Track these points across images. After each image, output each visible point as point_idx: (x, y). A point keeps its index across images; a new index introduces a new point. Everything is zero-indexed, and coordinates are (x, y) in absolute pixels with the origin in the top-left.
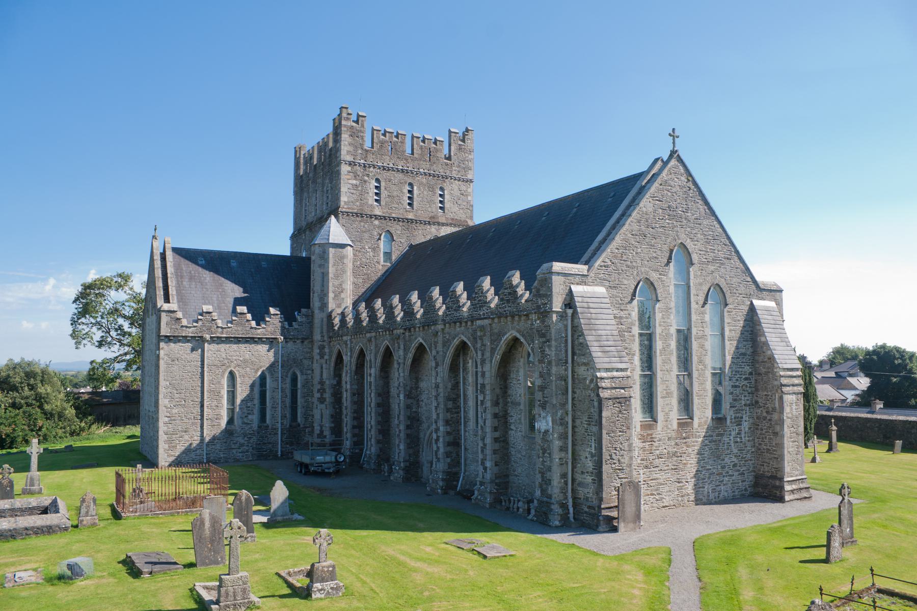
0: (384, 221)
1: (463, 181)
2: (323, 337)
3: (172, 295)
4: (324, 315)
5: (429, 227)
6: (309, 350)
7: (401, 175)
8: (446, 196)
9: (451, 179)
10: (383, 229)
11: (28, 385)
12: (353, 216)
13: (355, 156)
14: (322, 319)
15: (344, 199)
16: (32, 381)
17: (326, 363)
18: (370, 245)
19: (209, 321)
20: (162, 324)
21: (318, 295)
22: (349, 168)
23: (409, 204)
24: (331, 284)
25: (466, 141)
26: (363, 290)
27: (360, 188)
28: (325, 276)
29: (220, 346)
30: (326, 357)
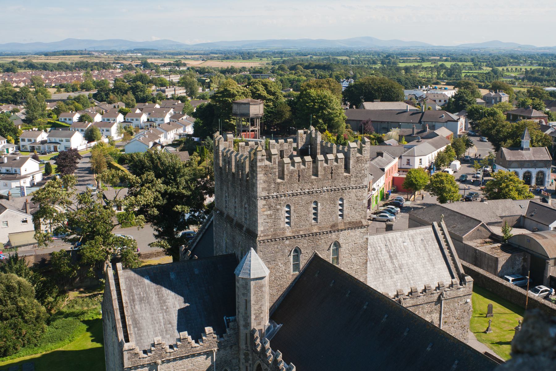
0: (293, 240)
1: (360, 188)
2: (248, 347)
3: (130, 334)
4: (248, 332)
5: (330, 235)
6: (236, 352)
7: (307, 197)
8: (345, 205)
9: (350, 189)
10: (293, 246)
11: (10, 298)
12: (268, 242)
13: (269, 191)
14: (246, 334)
15: (260, 228)
16: (12, 295)
17: (250, 366)
18: (282, 262)
19: (159, 350)
20: (125, 360)
21: (243, 316)
22: (264, 202)
23: (315, 219)
24: (252, 309)
25: (363, 152)
26: (277, 297)
27: (273, 217)
28: (247, 303)
29: (169, 364)
30: (250, 362)
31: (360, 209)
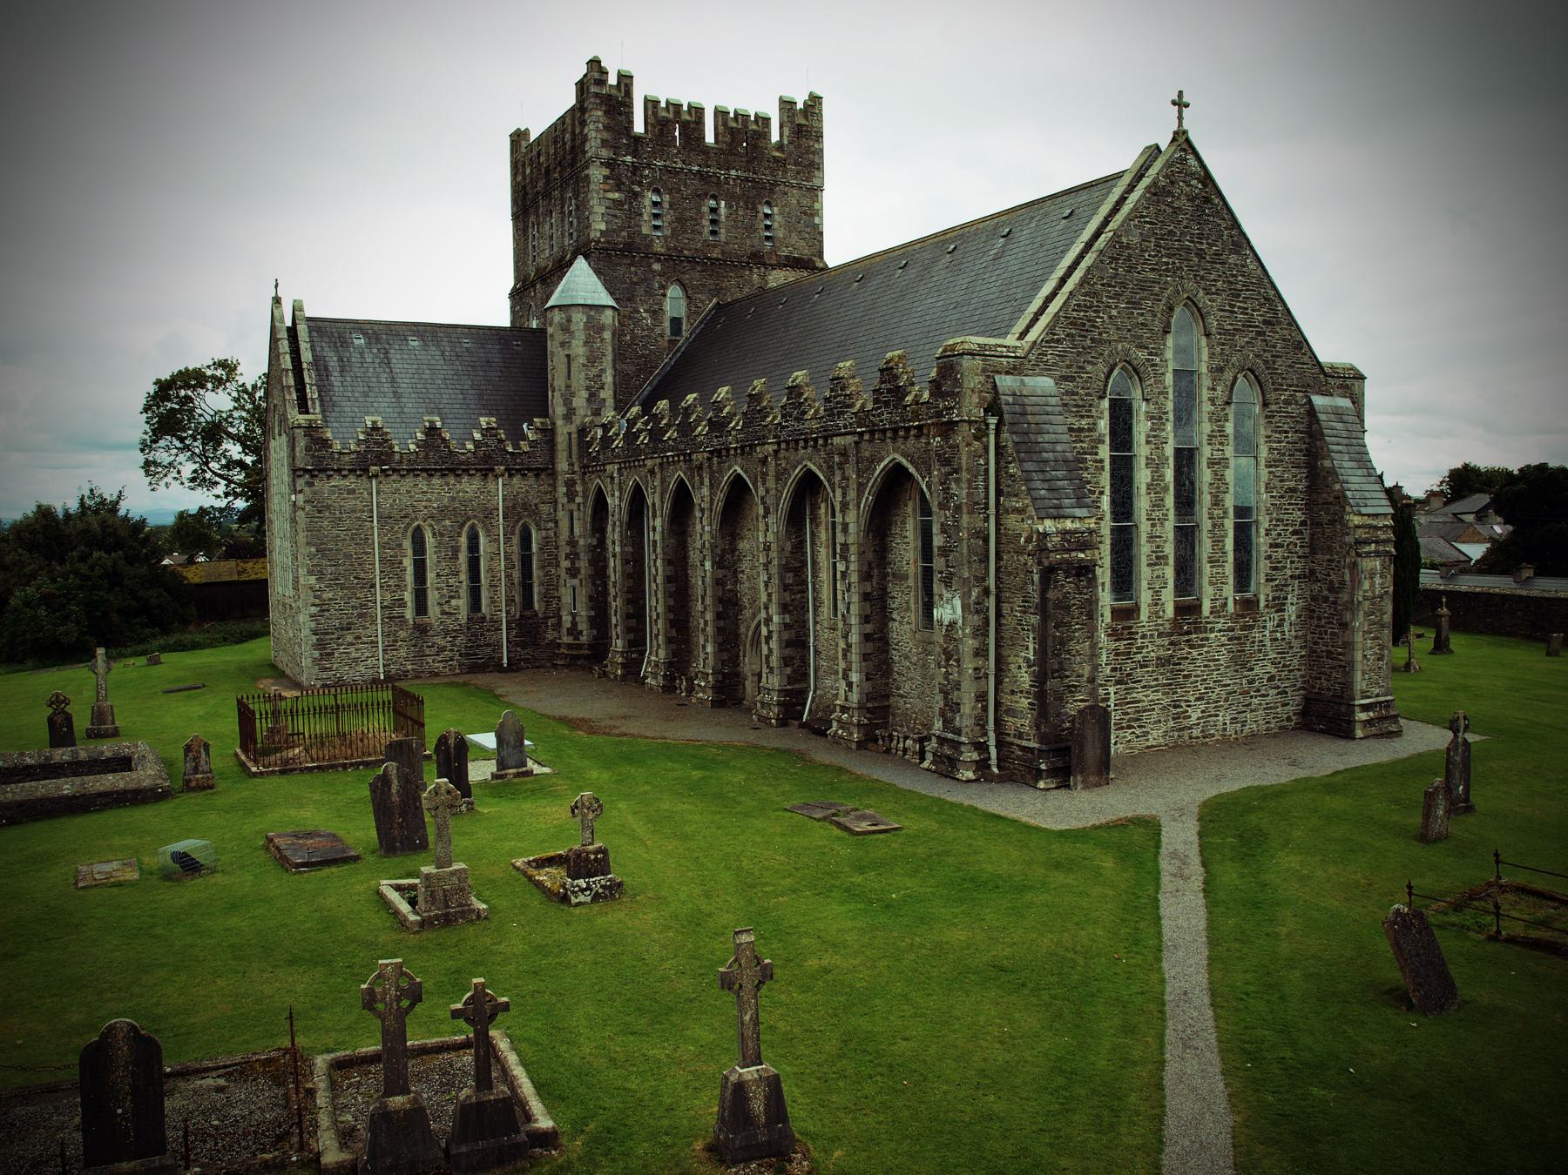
14: (570, 434)
30: (578, 500)
31: (809, 233)
